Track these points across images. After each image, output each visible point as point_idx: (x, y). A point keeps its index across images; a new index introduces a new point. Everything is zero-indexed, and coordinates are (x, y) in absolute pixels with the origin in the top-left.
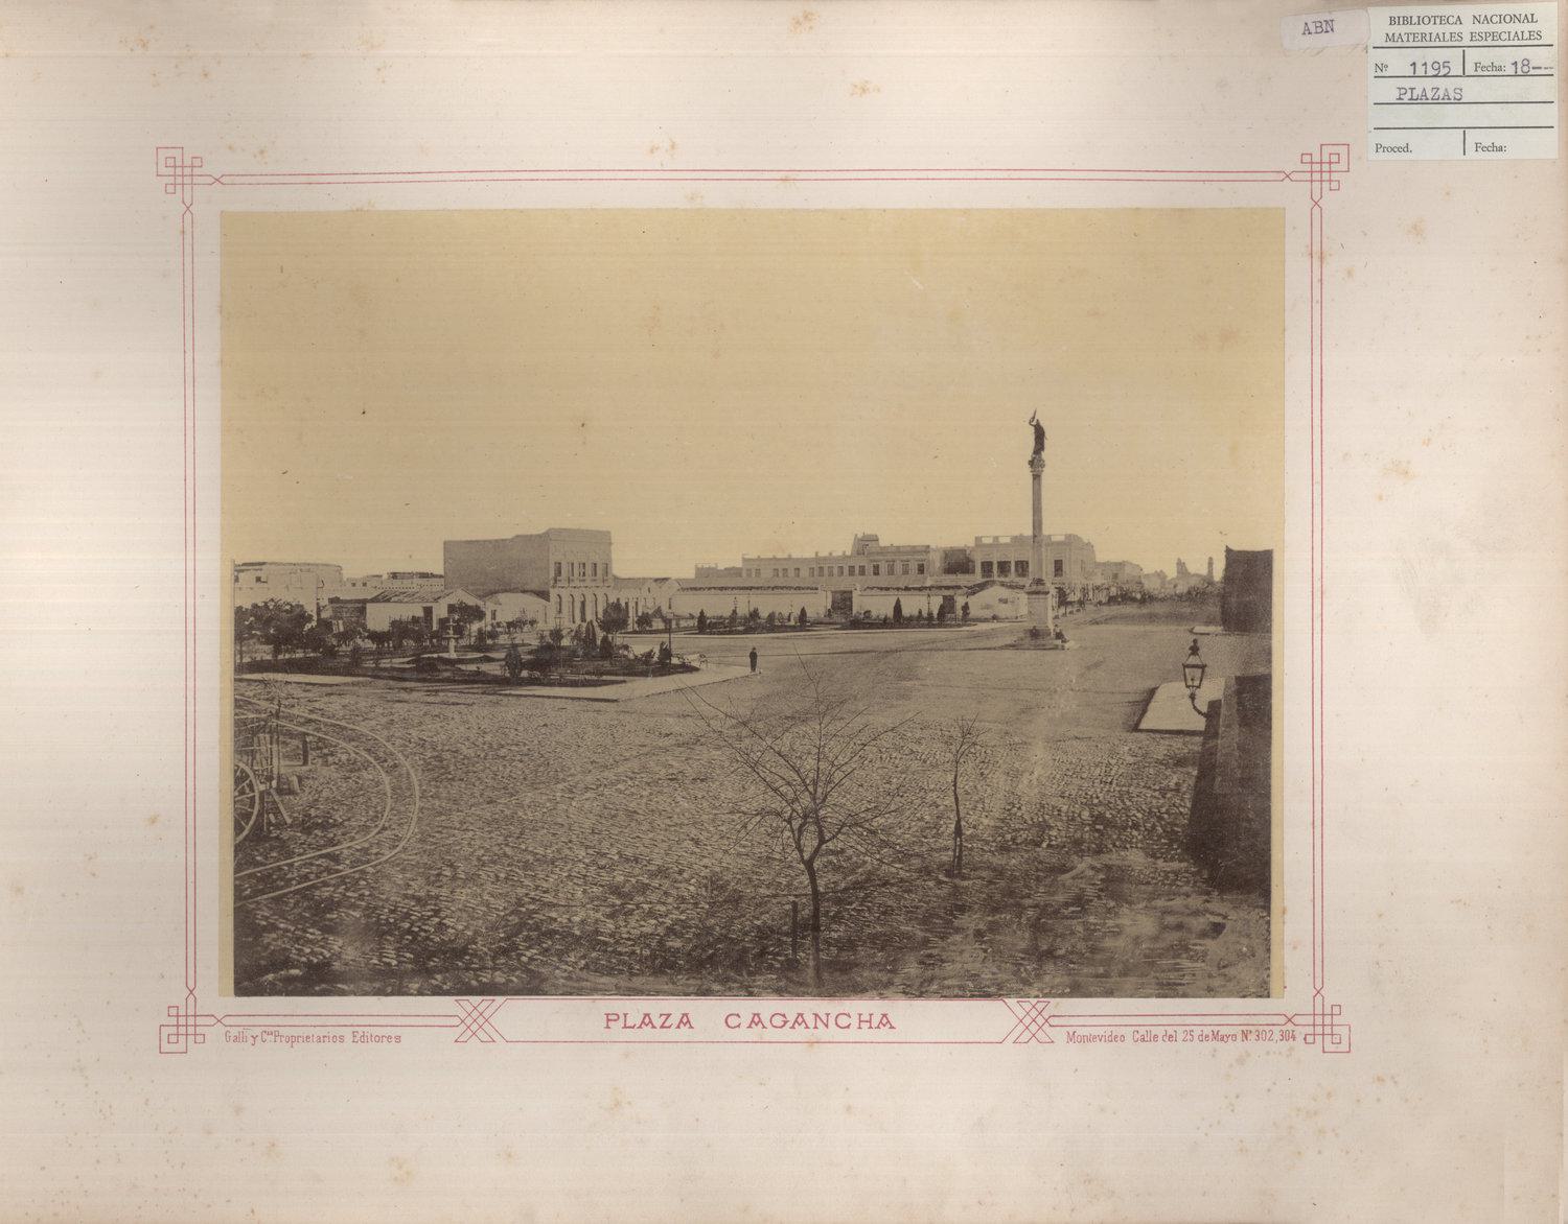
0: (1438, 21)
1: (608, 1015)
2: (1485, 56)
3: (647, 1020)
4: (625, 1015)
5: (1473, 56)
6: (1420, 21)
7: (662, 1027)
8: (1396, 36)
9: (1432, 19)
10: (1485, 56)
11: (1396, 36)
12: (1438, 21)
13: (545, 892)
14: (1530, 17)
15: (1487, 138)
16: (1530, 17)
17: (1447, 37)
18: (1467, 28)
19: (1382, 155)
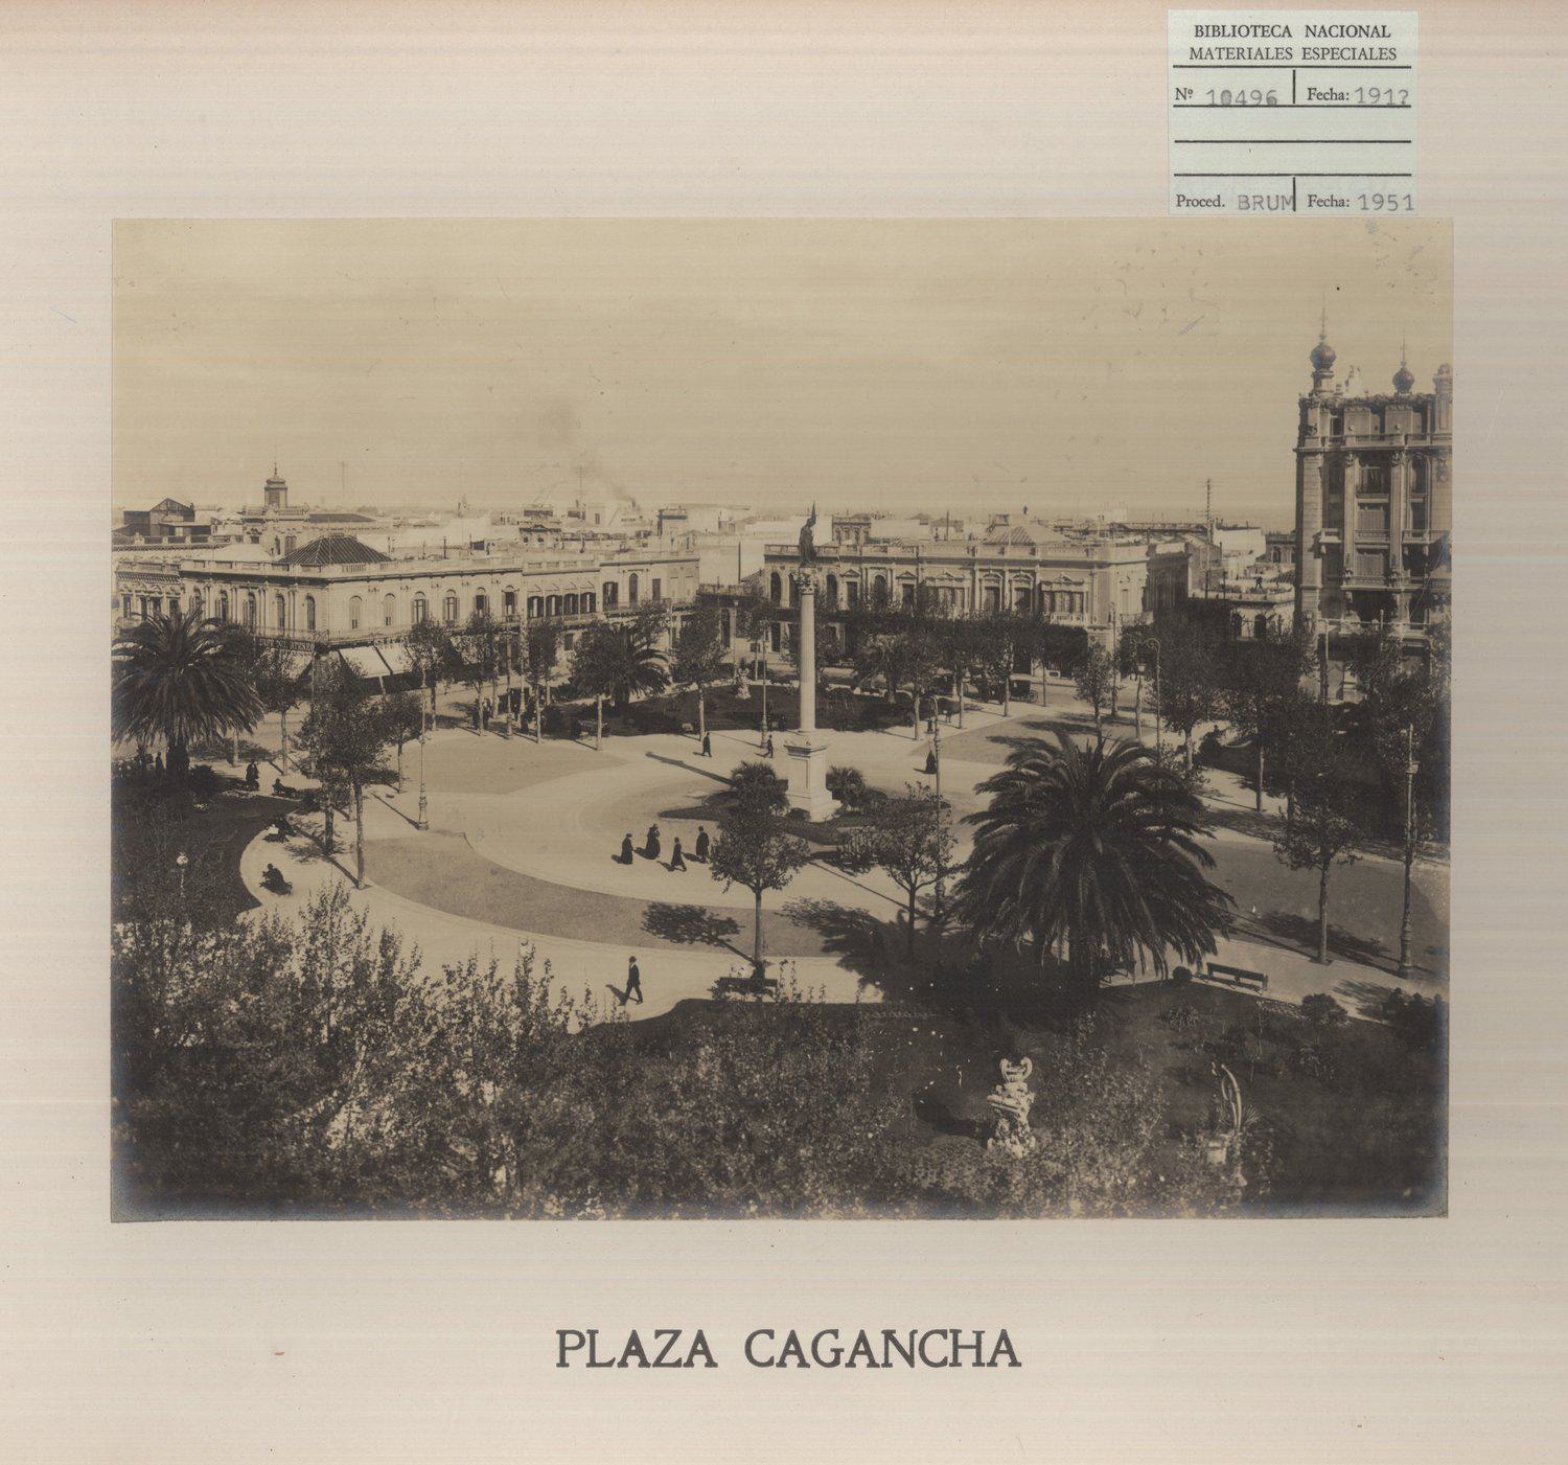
0: (1259, 31)
1: (562, 1334)
2: (1324, 80)
3: (700, 1347)
4: (593, 1333)
5: (1306, 79)
6: (1236, 31)
7: (658, 1363)
8: (1204, 51)
9: (1252, 30)
10: (1324, 80)
11: (1254, 52)
12: (1259, 31)
13: (359, 931)
14: (1380, 30)
15: (1322, 188)
16: (1380, 30)
17: (1272, 53)
18: (1298, 41)
19: (1184, 208)
